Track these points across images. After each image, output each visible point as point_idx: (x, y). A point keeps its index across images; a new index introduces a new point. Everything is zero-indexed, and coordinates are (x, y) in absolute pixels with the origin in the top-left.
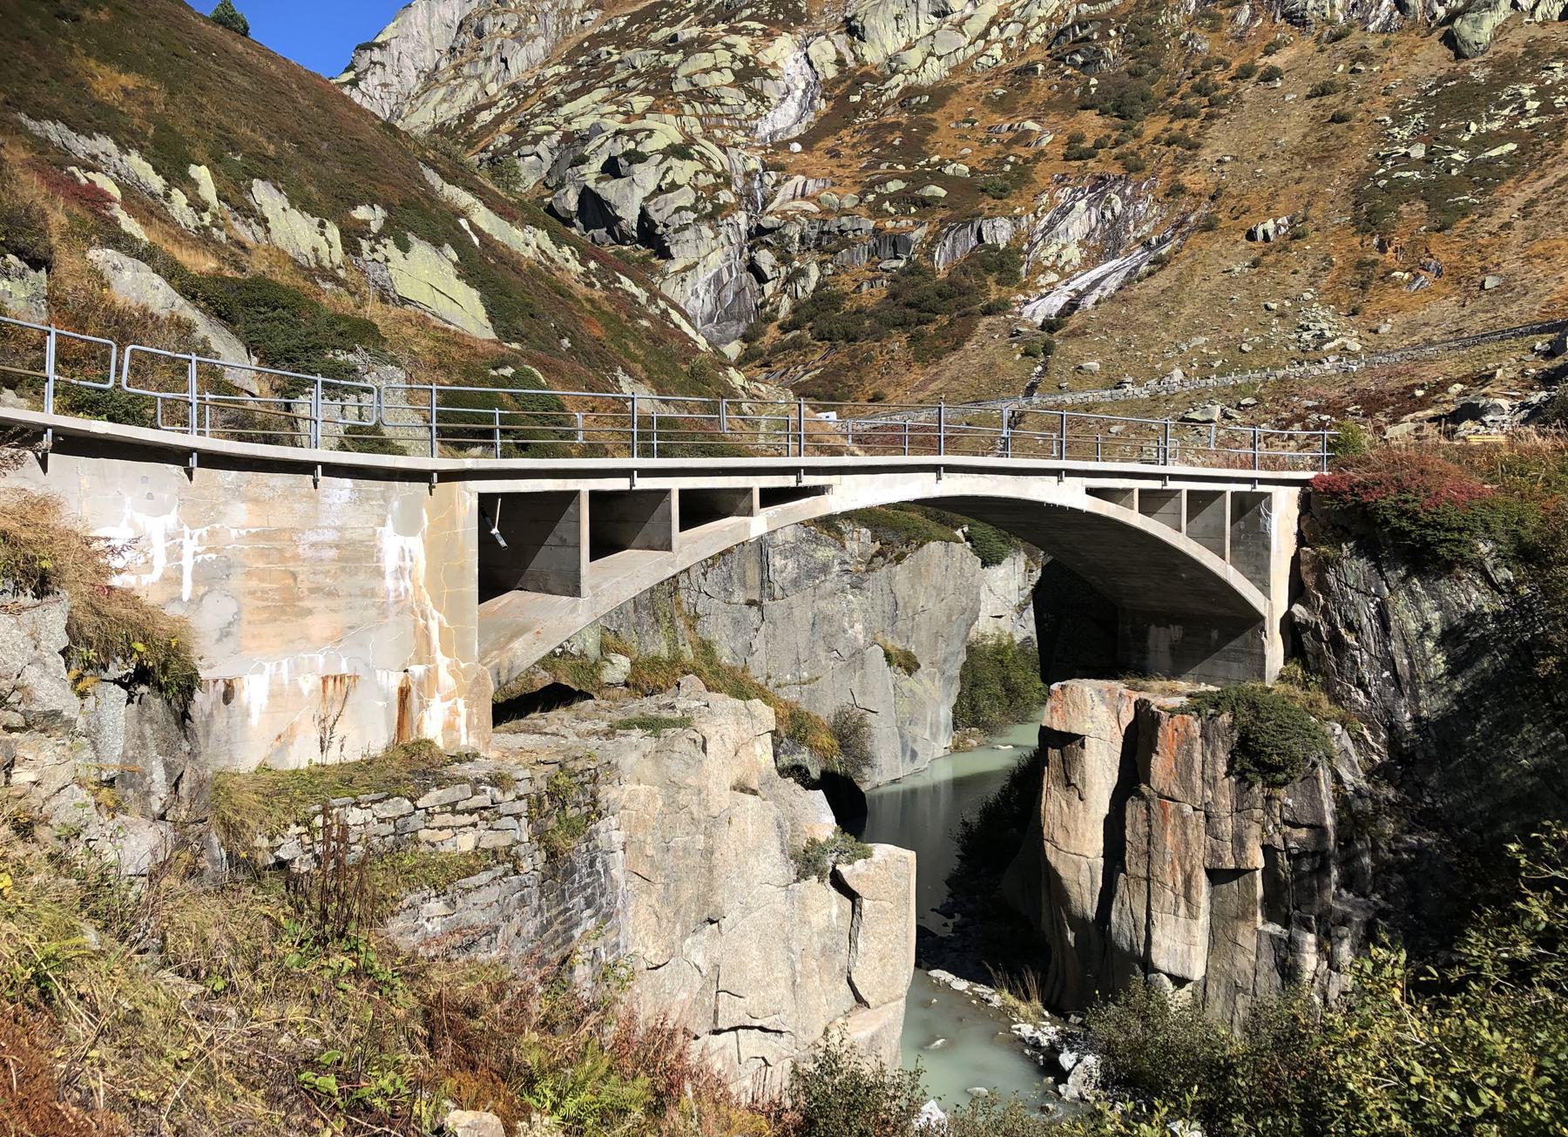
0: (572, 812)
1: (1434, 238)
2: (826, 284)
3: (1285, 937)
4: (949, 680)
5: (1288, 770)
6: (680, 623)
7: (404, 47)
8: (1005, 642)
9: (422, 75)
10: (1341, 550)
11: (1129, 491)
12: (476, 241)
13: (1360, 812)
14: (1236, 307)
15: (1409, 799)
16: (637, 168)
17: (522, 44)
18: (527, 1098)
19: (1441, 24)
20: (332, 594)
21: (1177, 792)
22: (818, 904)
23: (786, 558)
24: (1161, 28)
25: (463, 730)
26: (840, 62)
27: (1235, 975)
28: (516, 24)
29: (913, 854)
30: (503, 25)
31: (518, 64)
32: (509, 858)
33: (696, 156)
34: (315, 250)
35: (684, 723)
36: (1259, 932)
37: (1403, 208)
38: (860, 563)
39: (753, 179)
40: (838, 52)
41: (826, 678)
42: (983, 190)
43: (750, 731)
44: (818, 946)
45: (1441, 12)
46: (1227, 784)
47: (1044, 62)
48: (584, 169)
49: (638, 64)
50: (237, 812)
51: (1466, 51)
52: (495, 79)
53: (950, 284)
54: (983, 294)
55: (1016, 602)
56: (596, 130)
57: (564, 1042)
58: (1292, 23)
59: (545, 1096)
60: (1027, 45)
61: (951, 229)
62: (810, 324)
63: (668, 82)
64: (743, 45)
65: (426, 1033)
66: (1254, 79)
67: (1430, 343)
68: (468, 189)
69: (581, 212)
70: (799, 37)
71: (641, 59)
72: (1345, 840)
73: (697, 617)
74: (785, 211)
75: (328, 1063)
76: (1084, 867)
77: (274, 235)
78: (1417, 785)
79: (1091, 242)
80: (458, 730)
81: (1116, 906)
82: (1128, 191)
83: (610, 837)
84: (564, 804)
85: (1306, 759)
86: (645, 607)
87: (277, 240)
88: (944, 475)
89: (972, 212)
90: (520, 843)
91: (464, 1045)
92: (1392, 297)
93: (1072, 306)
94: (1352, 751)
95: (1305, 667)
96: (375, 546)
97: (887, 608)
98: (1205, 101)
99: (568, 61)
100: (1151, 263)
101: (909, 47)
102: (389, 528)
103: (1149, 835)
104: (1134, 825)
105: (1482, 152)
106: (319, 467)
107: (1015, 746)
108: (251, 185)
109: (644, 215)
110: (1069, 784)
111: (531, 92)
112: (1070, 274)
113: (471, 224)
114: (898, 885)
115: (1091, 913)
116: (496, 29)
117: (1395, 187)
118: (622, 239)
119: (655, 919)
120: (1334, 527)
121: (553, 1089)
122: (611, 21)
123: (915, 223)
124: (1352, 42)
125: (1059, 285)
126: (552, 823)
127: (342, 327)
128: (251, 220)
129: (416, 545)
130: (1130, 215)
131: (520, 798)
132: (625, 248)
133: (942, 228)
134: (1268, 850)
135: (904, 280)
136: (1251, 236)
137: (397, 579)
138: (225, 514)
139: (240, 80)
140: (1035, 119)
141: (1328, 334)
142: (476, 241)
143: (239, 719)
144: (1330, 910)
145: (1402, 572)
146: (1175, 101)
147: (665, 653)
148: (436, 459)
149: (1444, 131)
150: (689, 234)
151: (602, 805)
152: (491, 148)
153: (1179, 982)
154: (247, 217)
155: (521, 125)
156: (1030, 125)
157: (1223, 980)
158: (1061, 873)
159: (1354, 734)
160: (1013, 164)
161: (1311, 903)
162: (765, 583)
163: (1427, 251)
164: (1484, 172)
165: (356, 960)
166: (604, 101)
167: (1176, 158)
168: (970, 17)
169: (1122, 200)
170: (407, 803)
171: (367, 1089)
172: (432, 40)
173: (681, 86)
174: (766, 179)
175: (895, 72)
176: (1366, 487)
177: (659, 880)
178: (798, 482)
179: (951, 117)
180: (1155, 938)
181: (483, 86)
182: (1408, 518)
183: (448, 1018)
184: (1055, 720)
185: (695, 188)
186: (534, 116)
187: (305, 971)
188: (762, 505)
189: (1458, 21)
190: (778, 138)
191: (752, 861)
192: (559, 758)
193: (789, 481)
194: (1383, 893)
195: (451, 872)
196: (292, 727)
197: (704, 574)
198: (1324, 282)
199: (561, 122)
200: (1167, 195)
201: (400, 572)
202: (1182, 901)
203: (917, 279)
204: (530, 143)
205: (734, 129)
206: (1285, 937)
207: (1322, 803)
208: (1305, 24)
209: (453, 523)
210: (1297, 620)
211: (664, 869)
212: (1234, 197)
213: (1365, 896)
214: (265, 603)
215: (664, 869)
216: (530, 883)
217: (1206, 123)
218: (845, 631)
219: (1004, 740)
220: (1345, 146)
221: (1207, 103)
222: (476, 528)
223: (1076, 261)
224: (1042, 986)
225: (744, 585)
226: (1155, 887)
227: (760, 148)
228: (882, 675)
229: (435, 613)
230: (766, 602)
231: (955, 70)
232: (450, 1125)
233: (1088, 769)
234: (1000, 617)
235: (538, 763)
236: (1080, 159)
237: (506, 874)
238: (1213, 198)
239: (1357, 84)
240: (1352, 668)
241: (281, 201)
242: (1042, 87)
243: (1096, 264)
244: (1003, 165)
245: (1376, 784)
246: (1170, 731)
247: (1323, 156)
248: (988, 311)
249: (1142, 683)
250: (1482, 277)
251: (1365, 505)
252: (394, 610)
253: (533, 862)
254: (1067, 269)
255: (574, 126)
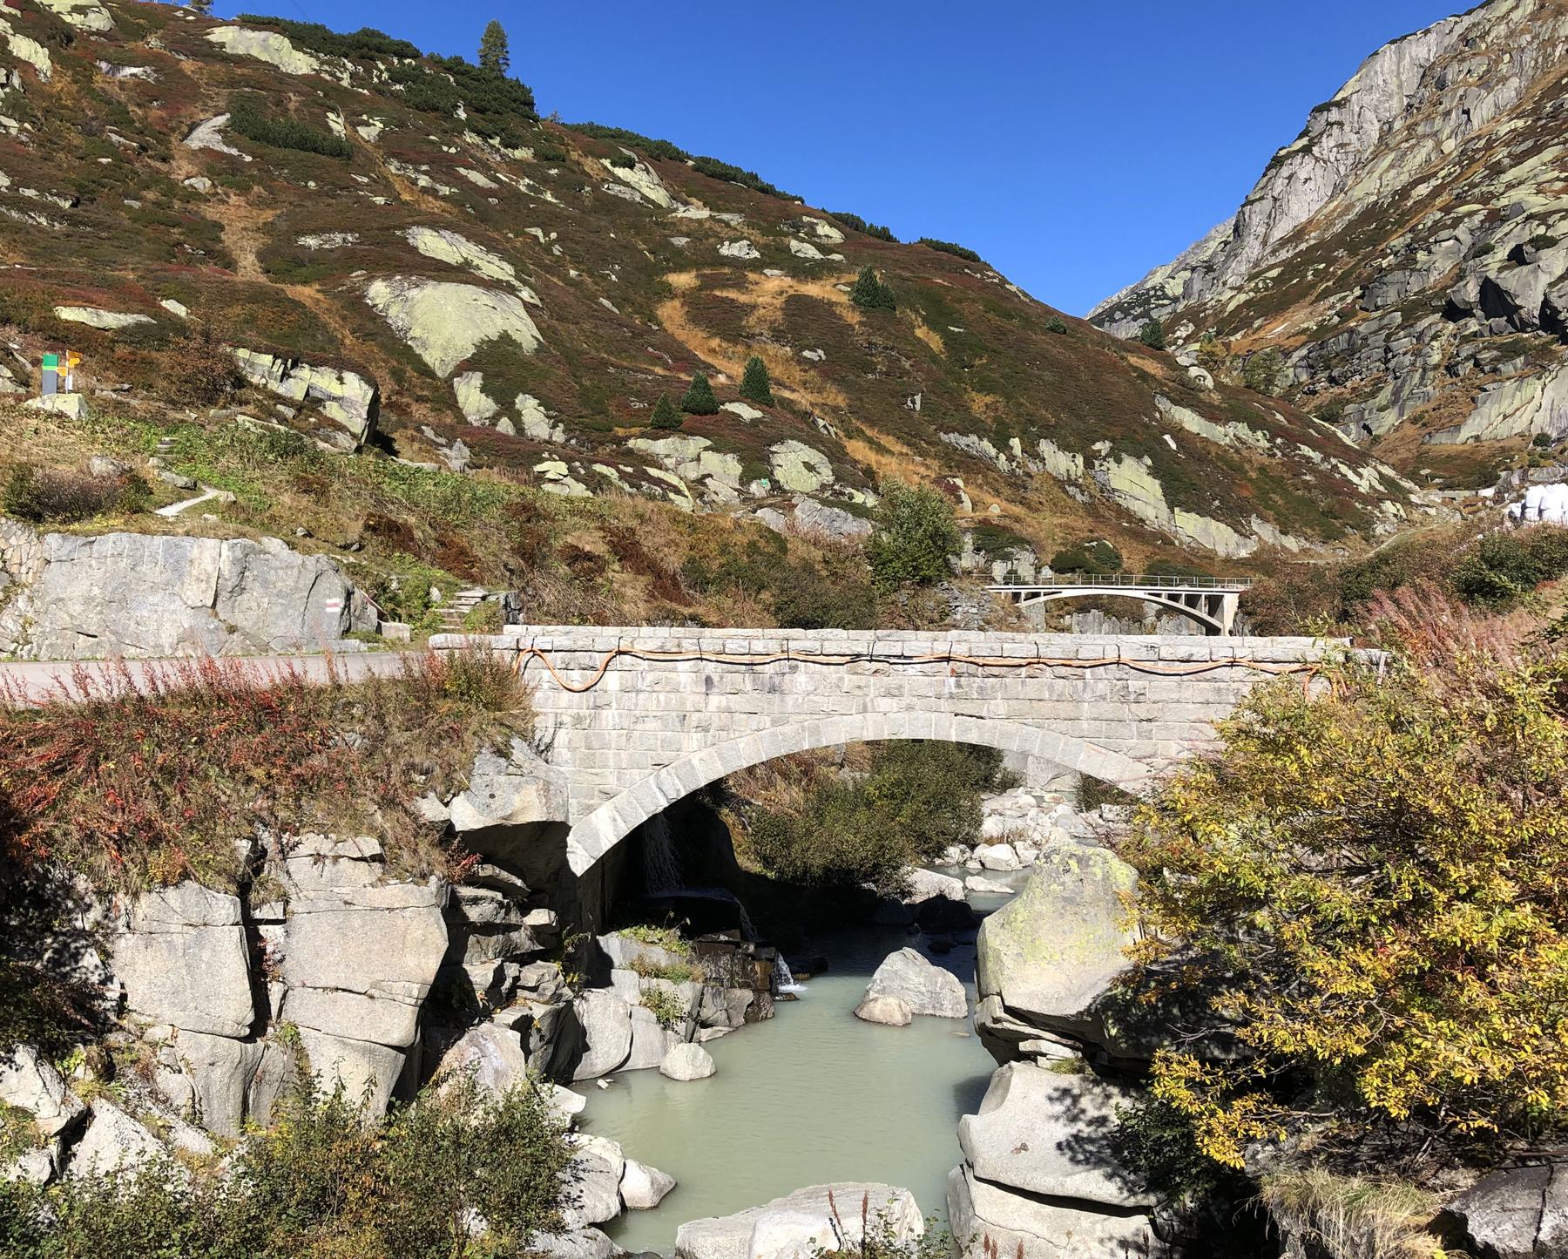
7: (1366, 99)
16: (1546, 254)
30: (1469, 71)
31: (1482, 112)
48: (1488, 259)
109: (1546, 303)
111: (1477, 156)
118: (1524, 326)
132: (1526, 335)
172: (1400, 86)
204: (1449, 227)
241: (1054, 448)
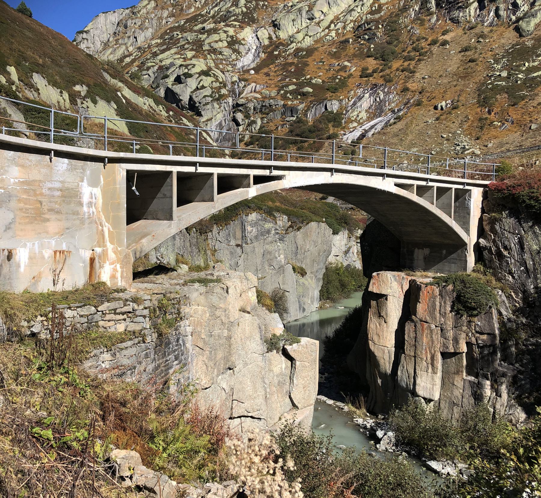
0: (169, 317)
1: (511, 108)
2: (264, 127)
3: (476, 382)
4: (318, 280)
5: (479, 310)
6: (209, 252)
7: (96, 32)
8: (340, 265)
9: (103, 44)
10: (502, 215)
11: (412, 185)
12: (124, 101)
13: (510, 328)
14: (429, 136)
15: (532, 323)
16: (189, 80)
17: (143, 31)
18: (150, 445)
19: (514, 23)
20: (58, 212)
21: (428, 319)
22: (277, 363)
23: (252, 227)
24: (400, 24)
25: (119, 278)
26: (270, 38)
27: (453, 399)
28: (140, 23)
29: (318, 342)
30: (135, 23)
31: (141, 39)
32: (140, 336)
33: (212, 75)
34: (58, 102)
35: (218, 280)
36: (464, 380)
37: (498, 96)
38: (283, 230)
39: (235, 85)
40: (269, 34)
41: (268, 277)
42: (328, 89)
43: (247, 286)
44: (276, 381)
45: (514, 18)
46: (451, 315)
47: (352, 38)
48: (167, 80)
49: (189, 39)
50: (12, 308)
51: (524, 34)
52: (132, 45)
53: (314, 127)
54: (327, 131)
55: (344, 250)
56: (172, 64)
57: (167, 420)
58: (453, 22)
59: (160, 444)
60: (345, 31)
61: (314, 105)
62: (257, 143)
63: (201, 46)
64: (231, 31)
65: (101, 413)
66: (438, 45)
67: (509, 151)
68: (121, 81)
69: (166, 97)
70: (254, 28)
71: (190, 37)
72: (504, 341)
73: (215, 251)
74: (248, 98)
75: (49, 423)
76: (386, 351)
77: (41, 95)
78: (535, 317)
79: (371, 111)
80: (117, 279)
81: (400, 368)
82: (386, 90)
83: (186, 329)
84: (166, 313)
85: (487, 305)
86: (194, 245)
87: (43, 98)
88: (334, 174)
89: (323, 98)
90: (145, 329)
91: (121, 420)
92: (493, 132)
93: (363, 136)
94: (506, 302)
95: (485, 266)
96: (79, 191)
97: (293, 249)
98: (418, 54)
99: (161, 37)
100: (395, 119)
101: (298, 32)
102: (85, 184)
103: (416, 338)
104: (409, 333)
105: (530, 74)
106: (53, 152)
107: (345, 307)
108: (32, 75)
109: (191, 99)
110: (380, 316)
112: (362, 123)
113: (122, 94)
114: (311, 355)
115: (389, 371)
116: (132, 25)
117: (495, 88)
119: (205, 367)
120: (499, 205)
121: (163, 441)
122: (178, 22)
123: (300, 102)
124: (477, 30)
125: (358, 128)
126: (160, 321)
127: (67, 122)
128: (32, 89)
129: (97, 191)
130: (387, 99)
131: (146, 308)
133: (311, 104)
134: (469, 344)
135: (295, 125)
136: (436, 108)
137: (89, 207)
138: (8, 172)
139: (28, 33)
140: (348, 61)
141: (467, 147)
142: (124, 101)
143: (15, 268)
144: (497, 370)
145: (530, 224)
146: (405, 54)
147: (202, 264)
148: (106, 151)
149: (515, 66)
150: (209, 106)
151: (182, 315)
152: (130, 72)
153: (428, 401)
154: (31, 88)
155: (142, 63)
156: (346, 63)
157: (448, 401)
158: (376, 354)
159: (507, 295)
160: (340, 79)
161: (488, 367)
162: (244, 237)
163: (508, 114)
164: (531, 82)
165: (68, 378)
166: (176, 53)
167: (405, 77)
168: (323, 20)
169: (383, 93)
170: (93, 308)
171: (68, 437)
172: (107, 30)
173: (206, 47)
174: (240, 84)
175: (292, 42)
176: (514, 187)
177: (207, 349)
178: (270, 173)
179: (315, 60)
180: (417, 382)
181: (127, 48)
182: (534, 200)
183: (112, 406)
184: (375, 288)
185: (212, 88)
186: (147, 59)
187: (43, 382)
188: (254, 184)
189: (521, 22)
190: (245, 69)
191: (248, 343)
192: (163, 292)
193: (266, 172)
194: (520, 363)
195: (114, 340)
196: (40, 273)
197: (219, 233)
198: (465, 127)
199: (158, 62)
200: (402, 92)
201: (90, 204)
202: (430, 366)
203: (302, 124)
204: (146, 70)
205: (227, 65)
206: (476, 382)
207: (494, 324)
208: (458, 23)
209: (115, 183)
210: (481, 245)
211: (210, 345)
212: (429, 92)
213: (512, 364)
214: (27, 215)
215: (210, 345)
216: (150, 347)
217: (418, 63)
218: (276, 258)
219: (340, 305)
220: (474, 72)
221: (418, 55)
222: (126, 186)
223: (365, 118)
224: (366, 402)
225: (235, 238)
226: (418, 360)
227: (238, 72)
228: (291, 276)
229: (107, 224)
230: (244, 245)
231: (316, 42)
232: (113, 457)
233: (389, 309)
234: (337, 256)
235: (153, 294)
236: (366, 77)
237: (139, 343)
238: (420, 93)
239: (479, 47)
240: (507, 266)
242: (351, 48)
243: (372, 119)
244: (335, 80)
245: (517, 317)
246: (425, 292)
247: (466, 76)
248: (329, 138)
249: (412, 273)
250: (530, 124)
251: (514, 195)
252: (87, 221)
253: (151, 338)
254: (361, 121)
255: (163, 63)
